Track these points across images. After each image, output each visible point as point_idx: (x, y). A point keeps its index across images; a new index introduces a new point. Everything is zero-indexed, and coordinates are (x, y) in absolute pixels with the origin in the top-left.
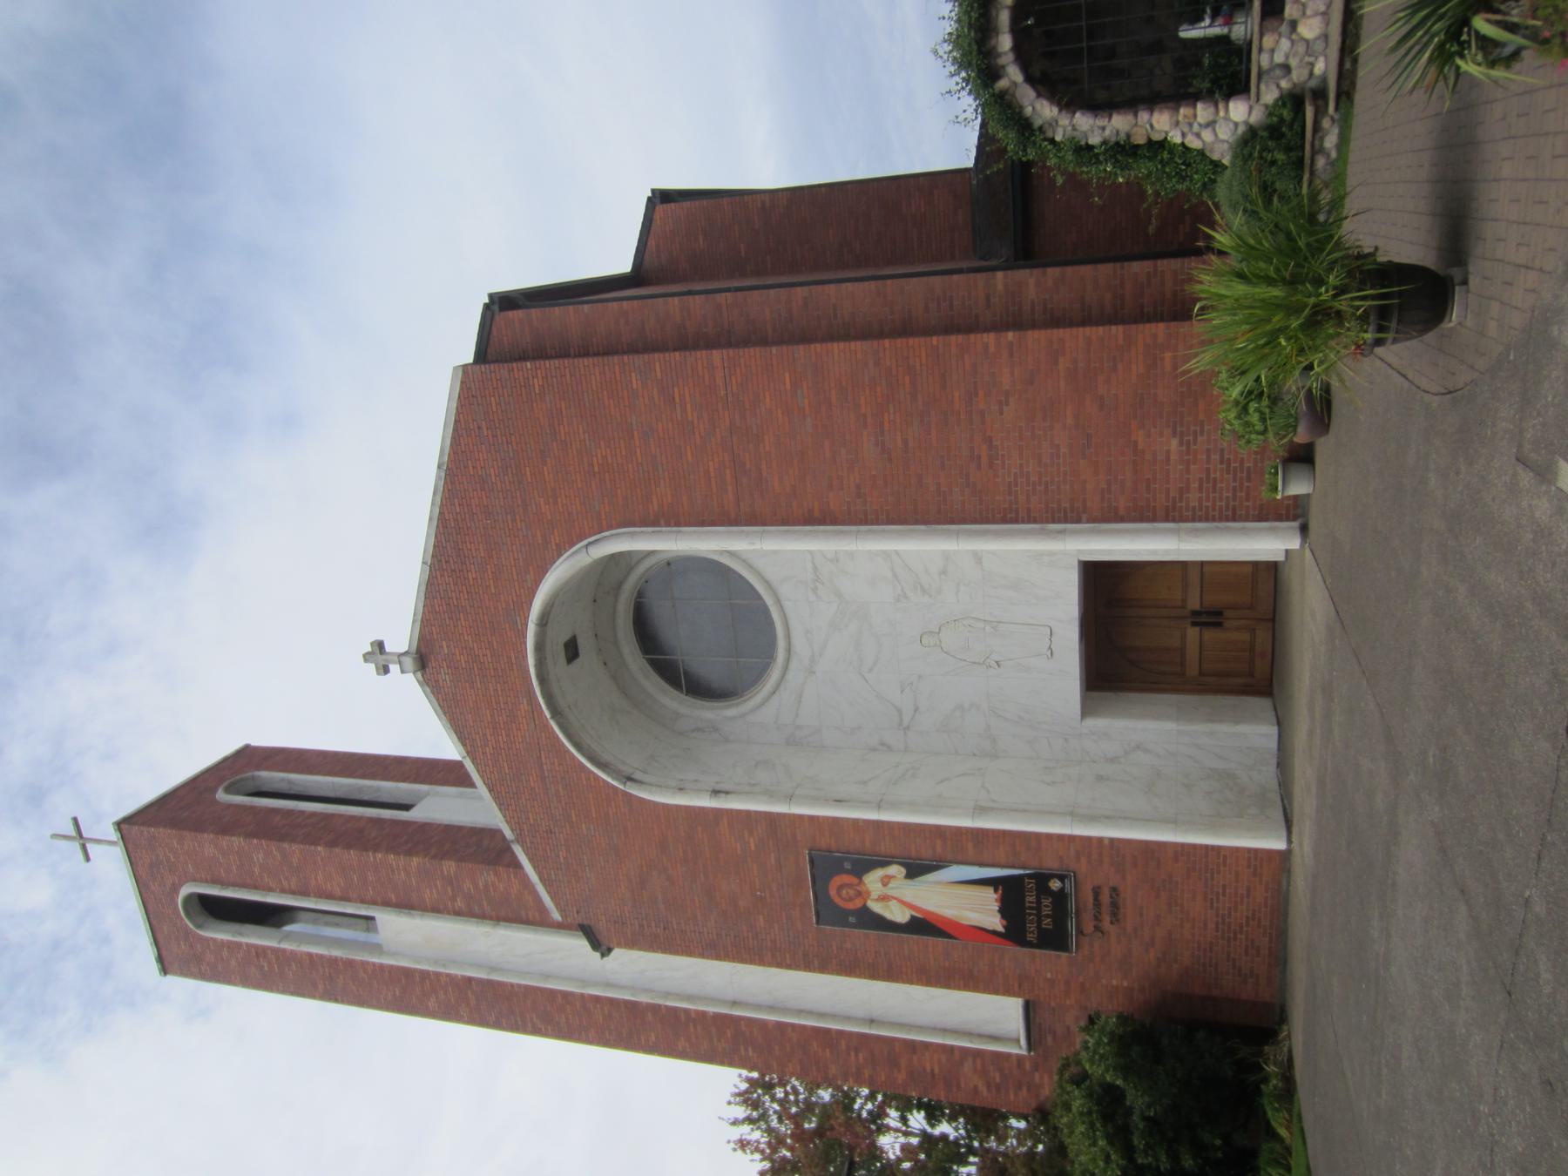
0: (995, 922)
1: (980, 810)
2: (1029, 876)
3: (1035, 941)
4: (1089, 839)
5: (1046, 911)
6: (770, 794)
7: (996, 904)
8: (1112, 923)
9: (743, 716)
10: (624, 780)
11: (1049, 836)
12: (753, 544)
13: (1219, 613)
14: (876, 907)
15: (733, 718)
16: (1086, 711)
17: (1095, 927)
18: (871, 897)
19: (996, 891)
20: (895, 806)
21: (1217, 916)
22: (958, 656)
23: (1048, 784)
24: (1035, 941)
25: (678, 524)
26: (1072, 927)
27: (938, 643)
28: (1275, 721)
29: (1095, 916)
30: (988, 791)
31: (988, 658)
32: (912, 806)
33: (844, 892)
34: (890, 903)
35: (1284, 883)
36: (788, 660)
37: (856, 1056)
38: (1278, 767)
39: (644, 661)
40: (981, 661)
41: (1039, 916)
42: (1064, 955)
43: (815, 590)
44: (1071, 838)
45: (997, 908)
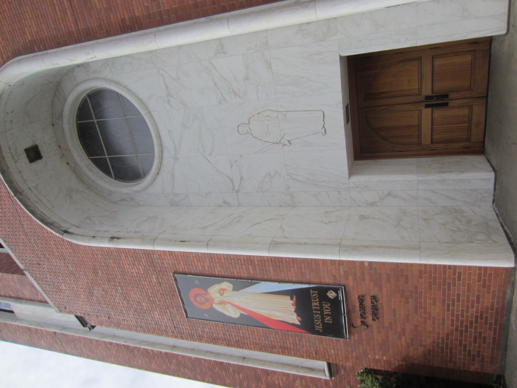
0: (294, 319)
1: (275, 245)
2: (314, 289)
3: (321, 331)
4: (354, 262)
5: (326, 312)
6: (143, 239)
7: (293, 307)
8: (373, 320)
9: (144, 189)
10: (62, 233)
11: (324, 261)
12: (88, 53)
13: (446, 96)
14: (219, 308)
15: (138, 192)
16: (351, 173)
17: (361, 322)
18: (215, 302)
19: (292, 299)
20: (218, 244)
21: (453, 316)
22: (263, 140)
23: (326, 223)
24: (321, 331)
25: (45, 49)
26: (344, 320)
27: (249, 130)
28: (491, 169)
29: (361, 315)
30: (283, 231)
31: (282, 138)
32: (229, 244)
33: (198, 298)
34: (227, 306)
35: (509, 292)
36: (162, 152)
37: (239, 375)
38: (493, 202)
39: (89, 160)
40: (278, 141)
41: (322, 315)
42: (341, 340)
43: (169, 102)
44: (341, 262)
45: (294, 310)
